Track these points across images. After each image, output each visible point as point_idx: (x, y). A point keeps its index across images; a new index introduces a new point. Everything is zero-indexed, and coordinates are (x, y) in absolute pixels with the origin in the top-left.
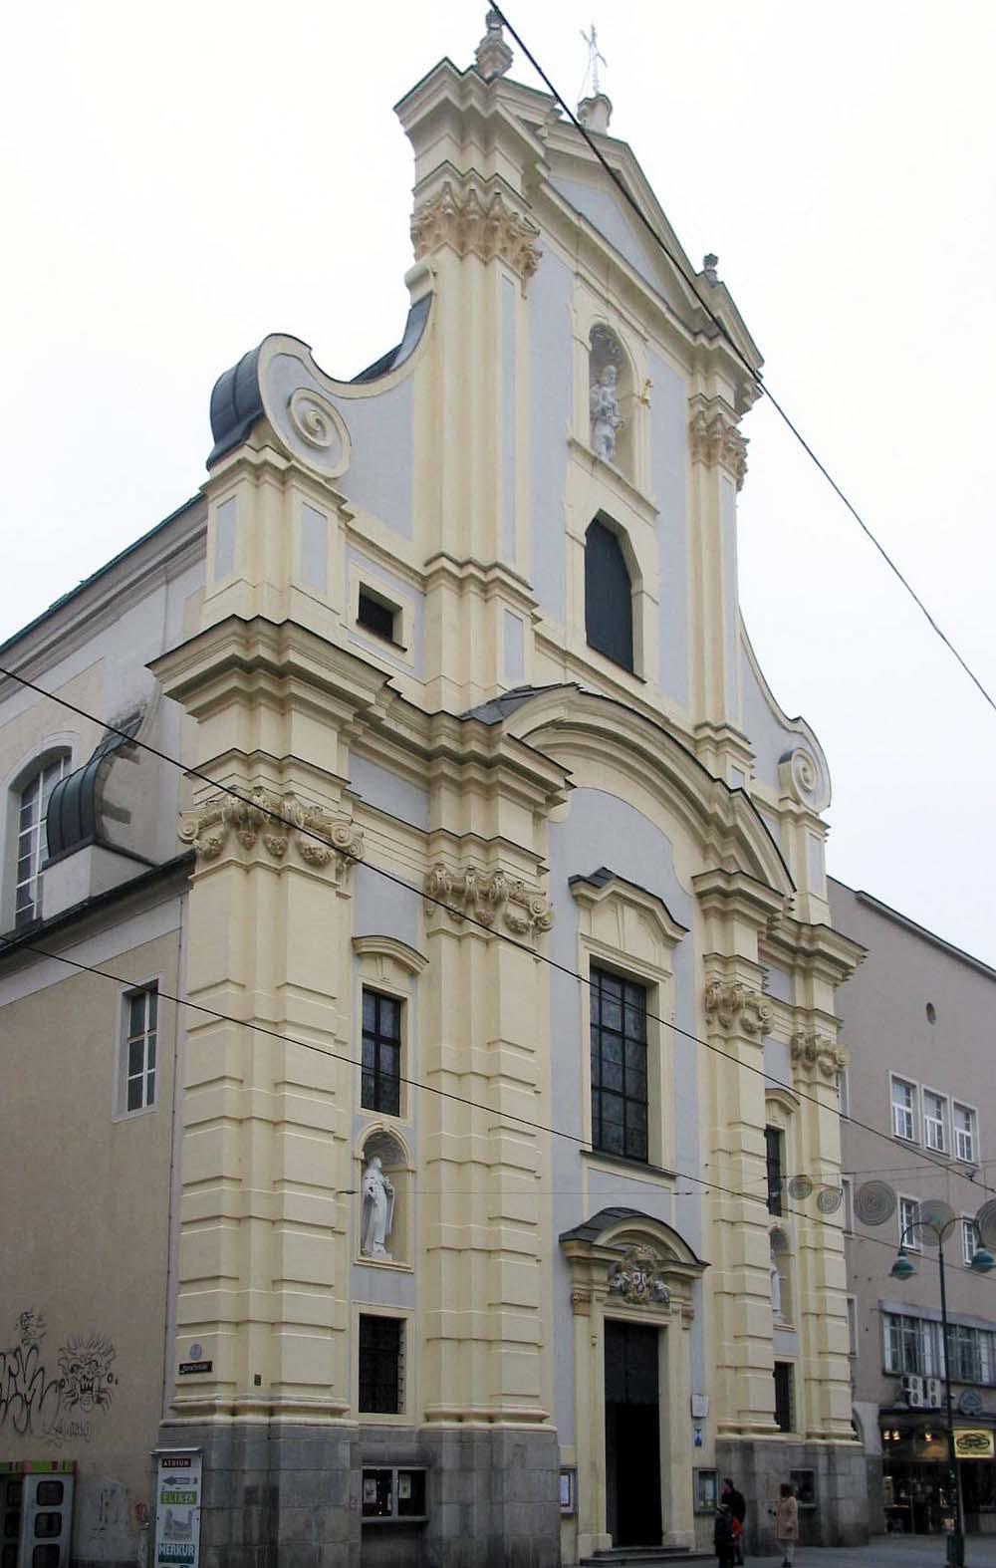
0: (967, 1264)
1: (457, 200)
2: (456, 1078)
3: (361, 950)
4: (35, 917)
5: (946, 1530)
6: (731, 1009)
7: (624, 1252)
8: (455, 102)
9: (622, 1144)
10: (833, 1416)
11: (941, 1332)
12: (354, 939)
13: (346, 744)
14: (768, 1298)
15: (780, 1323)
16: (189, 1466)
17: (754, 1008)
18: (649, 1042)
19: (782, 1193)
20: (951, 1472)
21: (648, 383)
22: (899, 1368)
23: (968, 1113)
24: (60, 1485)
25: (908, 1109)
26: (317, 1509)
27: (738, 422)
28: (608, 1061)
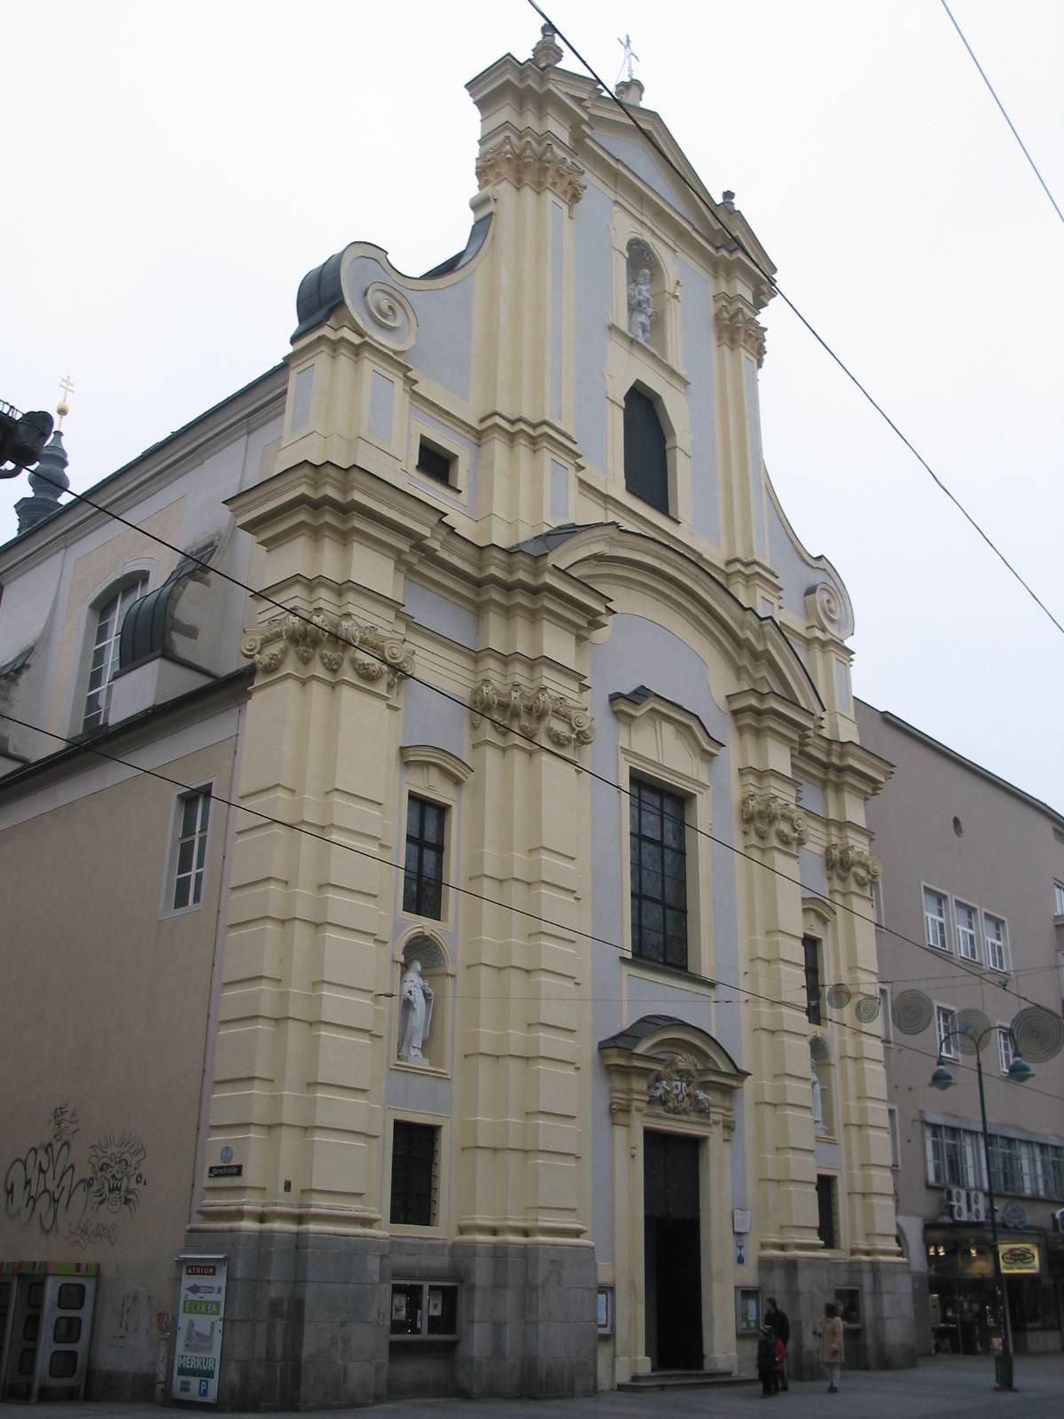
0: (1004, 1073)
1: (515, 148)
2: (498, 883)
3: (408, 759)
4: (101, 723)
5: (995, 1350)
6: (767, 820)
7: (663, 1060)
8: (515, 82)
9: (662, 952)
10: (878, 1230)
11: (982, 1143)
12: (402, 748)
13: (402, 572)
14: (809, 1108)
15: (822, 1134)
16: (214, 1274)
17: (789, 820)
18: (687, 852)
19: (821, 1002)
20: (997, 1288)
21: (678, 283)
22: (942, 1181)
23: (998, 923)
24: (82, 1288)
25: (972, 932)
26: (343, 1324)
27: (757, 314)
28: (648, 870)
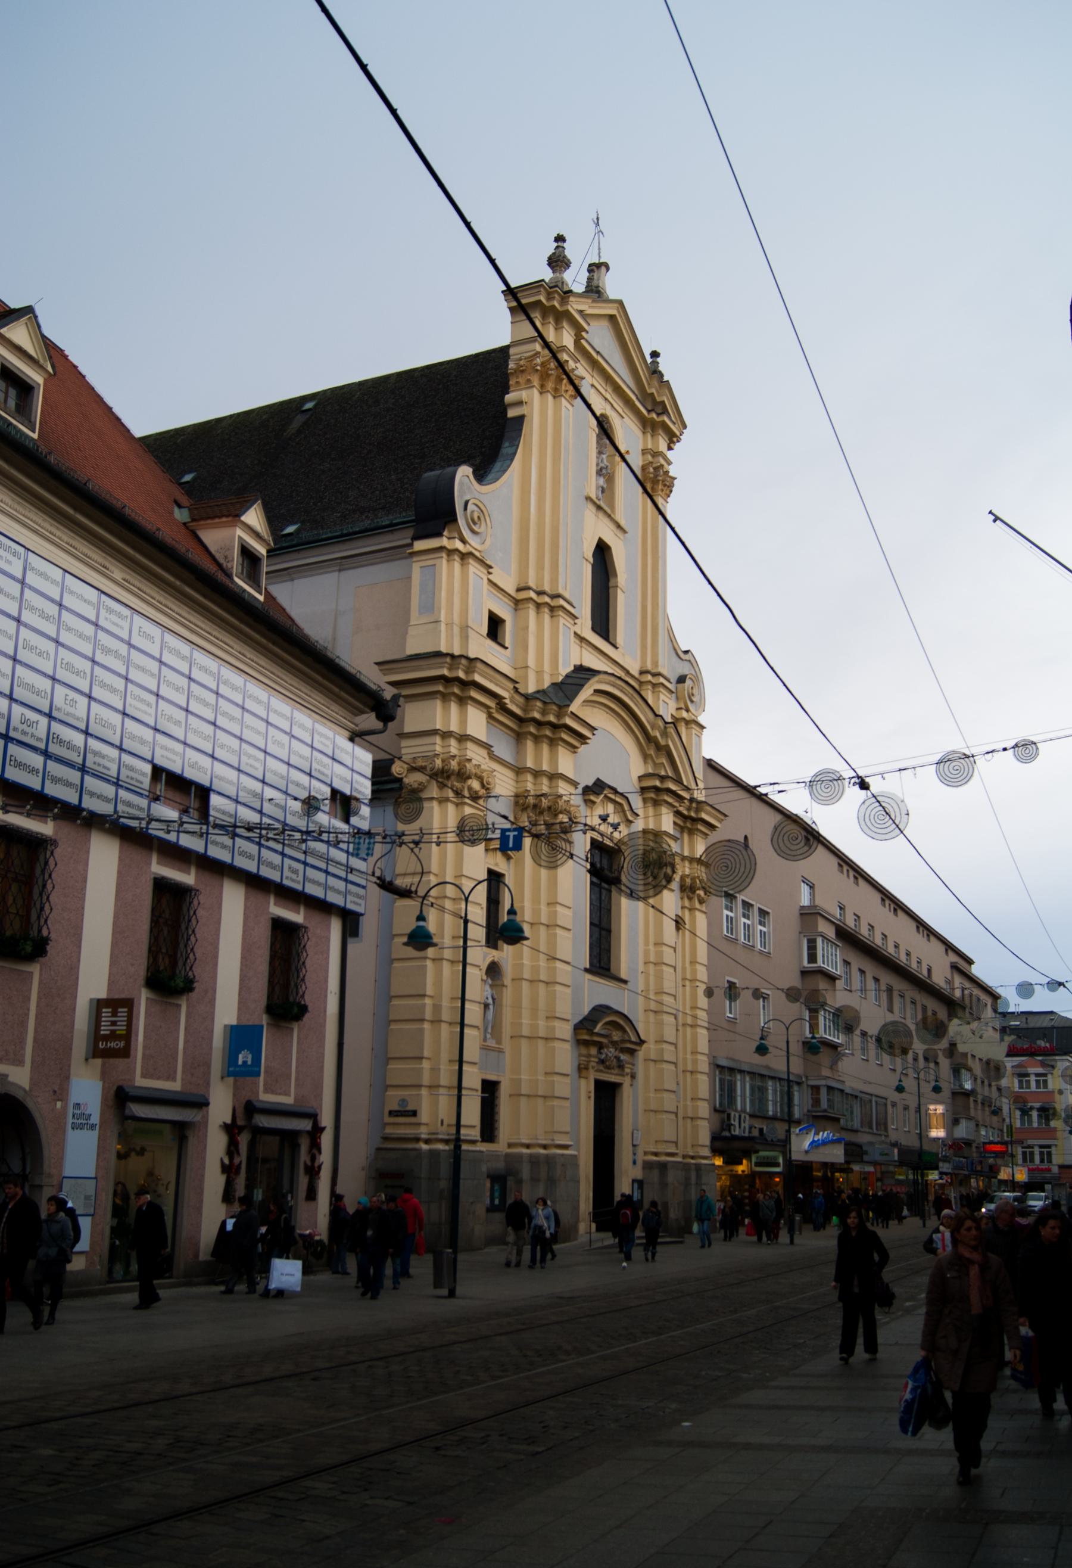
25: (731, 914)
